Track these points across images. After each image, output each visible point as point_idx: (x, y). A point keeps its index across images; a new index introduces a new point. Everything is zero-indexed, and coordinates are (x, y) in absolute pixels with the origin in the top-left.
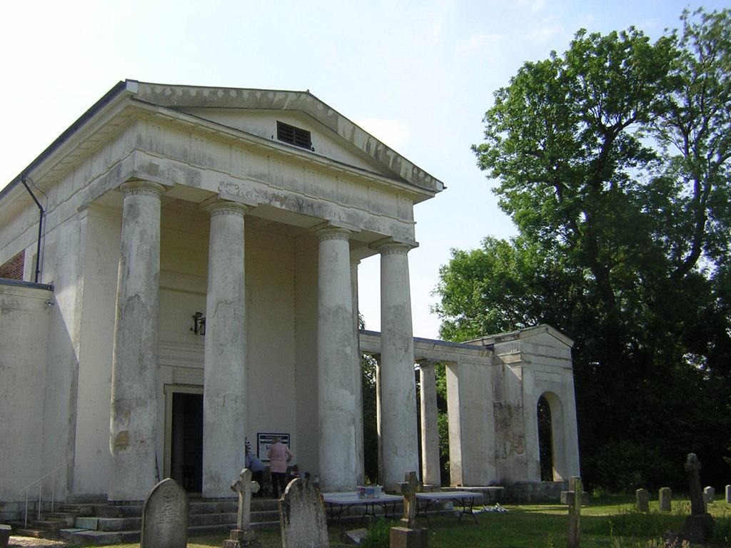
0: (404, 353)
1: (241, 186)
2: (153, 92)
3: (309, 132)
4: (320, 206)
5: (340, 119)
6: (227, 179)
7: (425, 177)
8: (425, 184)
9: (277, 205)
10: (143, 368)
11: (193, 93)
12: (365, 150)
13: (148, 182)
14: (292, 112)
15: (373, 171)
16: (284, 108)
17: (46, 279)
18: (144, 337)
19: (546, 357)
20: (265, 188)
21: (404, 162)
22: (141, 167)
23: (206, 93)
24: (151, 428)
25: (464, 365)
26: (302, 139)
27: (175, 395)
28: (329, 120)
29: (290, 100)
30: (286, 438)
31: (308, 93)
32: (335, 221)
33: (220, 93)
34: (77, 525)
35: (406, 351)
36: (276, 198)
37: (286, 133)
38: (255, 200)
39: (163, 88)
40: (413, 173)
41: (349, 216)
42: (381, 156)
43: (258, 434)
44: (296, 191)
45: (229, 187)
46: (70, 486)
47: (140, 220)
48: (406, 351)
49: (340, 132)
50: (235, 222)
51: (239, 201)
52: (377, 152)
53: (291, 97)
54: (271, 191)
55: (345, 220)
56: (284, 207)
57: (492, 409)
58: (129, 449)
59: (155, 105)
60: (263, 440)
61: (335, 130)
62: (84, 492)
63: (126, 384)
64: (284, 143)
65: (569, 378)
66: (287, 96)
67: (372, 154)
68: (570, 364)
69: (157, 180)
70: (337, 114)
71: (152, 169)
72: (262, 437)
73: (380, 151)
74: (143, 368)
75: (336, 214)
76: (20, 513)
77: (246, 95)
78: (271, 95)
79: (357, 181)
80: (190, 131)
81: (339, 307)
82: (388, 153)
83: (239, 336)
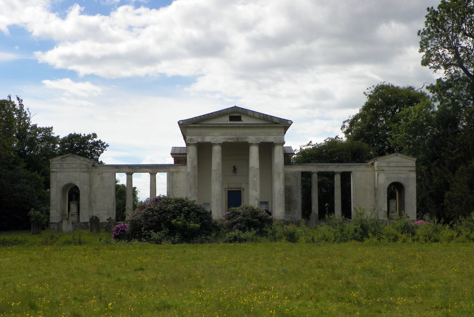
0: (278, 178)
2: (187, 121)
4: (245, 138)
5: (248, 111)
6: (212, 137)
9: (230, 141)
10: (191, 190)
11: (198, 118)
14: (230, 113)
16: (229, 112)
19: (395, 167)
21: (274, 118)
23: (202, 117)
26: (239, 119)
27: (228, 191)
28: (245, 112)
30: (267, 203)
35: (279, 177)
36: (229, 139)
37: (232, 118)
38: (221, 141)
48: (279, 177)
49: (249, 115)
51: (217, 143)
52: (263, 117)
54: (227, 137)
56: (232, 141)
65: (413, 175)
67: (262, 118)
68: (414, 169)
75: (251, 139)
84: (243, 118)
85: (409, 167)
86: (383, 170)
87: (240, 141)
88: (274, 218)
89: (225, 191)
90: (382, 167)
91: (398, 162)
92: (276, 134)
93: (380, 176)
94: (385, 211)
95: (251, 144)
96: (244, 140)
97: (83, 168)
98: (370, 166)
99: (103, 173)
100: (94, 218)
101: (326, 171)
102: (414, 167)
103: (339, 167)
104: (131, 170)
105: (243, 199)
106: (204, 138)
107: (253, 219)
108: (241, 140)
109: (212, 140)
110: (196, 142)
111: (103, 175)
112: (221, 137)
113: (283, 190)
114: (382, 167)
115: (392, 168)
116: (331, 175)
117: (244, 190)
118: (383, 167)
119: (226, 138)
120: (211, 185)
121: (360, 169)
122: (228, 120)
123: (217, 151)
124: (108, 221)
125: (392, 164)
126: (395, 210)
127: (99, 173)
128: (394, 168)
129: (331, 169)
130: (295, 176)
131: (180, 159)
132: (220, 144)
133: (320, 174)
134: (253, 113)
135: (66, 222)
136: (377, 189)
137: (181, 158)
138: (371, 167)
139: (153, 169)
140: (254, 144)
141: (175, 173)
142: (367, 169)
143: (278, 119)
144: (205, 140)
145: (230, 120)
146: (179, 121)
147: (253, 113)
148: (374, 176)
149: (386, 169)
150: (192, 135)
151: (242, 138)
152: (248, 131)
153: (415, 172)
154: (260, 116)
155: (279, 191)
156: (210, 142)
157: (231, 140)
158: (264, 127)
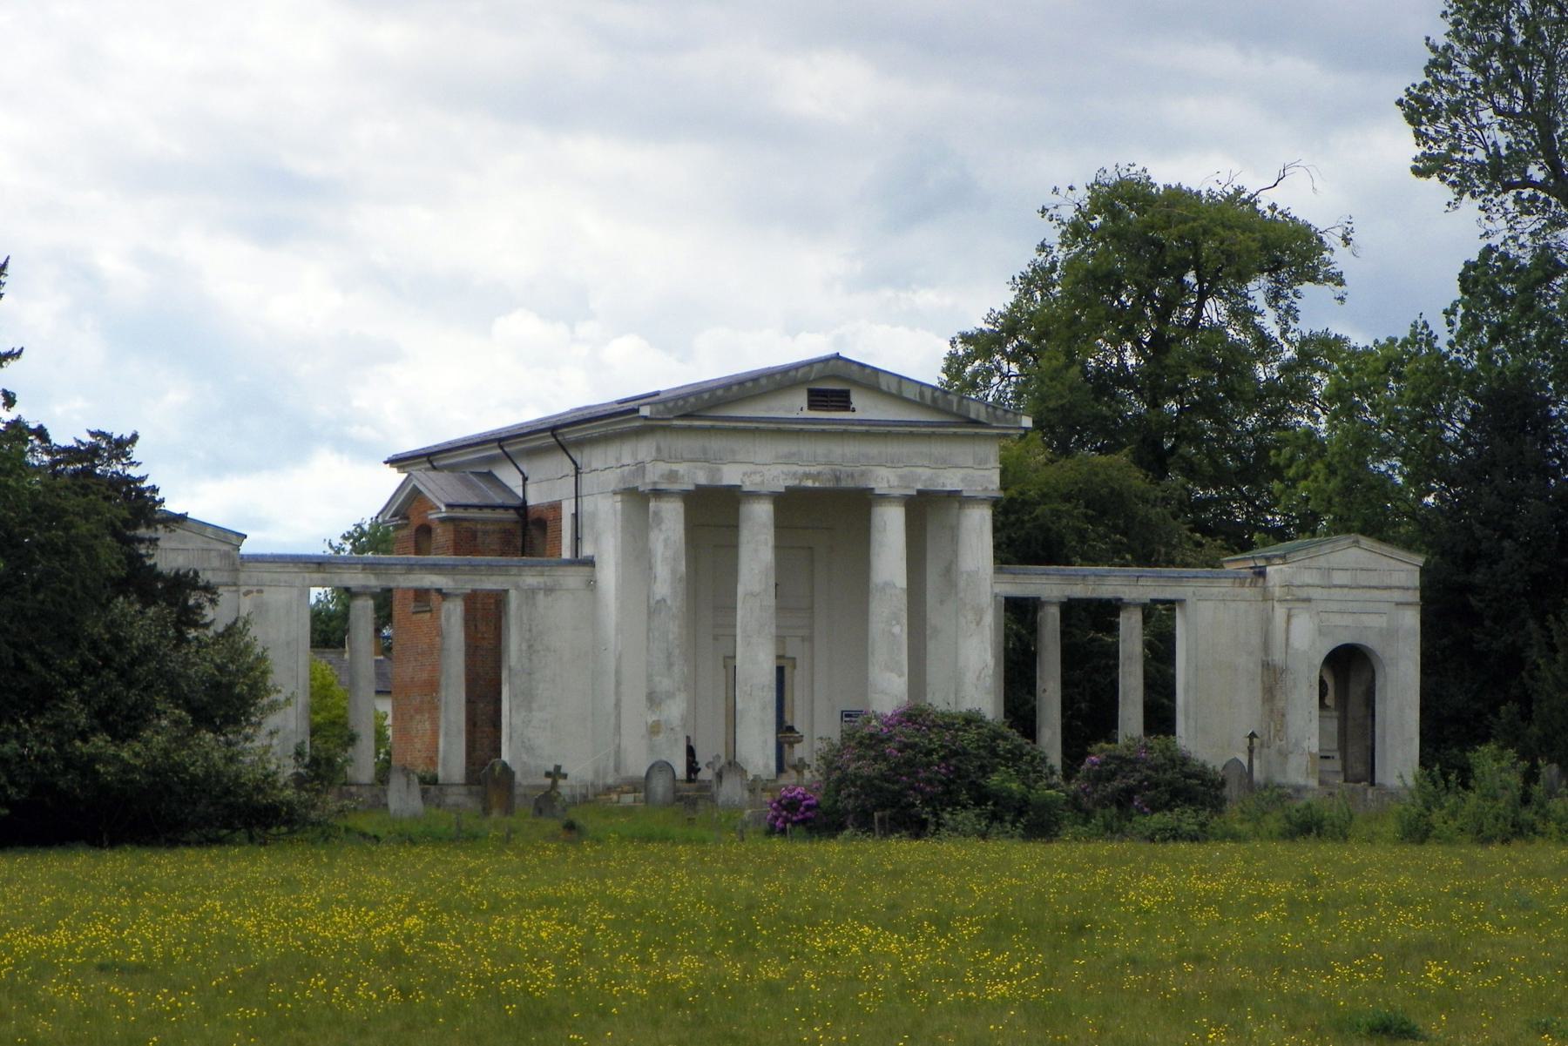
0: (973, 626)
4: (863, 474)
6: (751, 468)
9: (809, 483)
10: (670, 665)
17: (587, 550)
18: (671, 637)
19: (1350, 587)
22: (662, 476)
23: (720, 392)
25: (1200, 604)
26: (840, 400)
28: (871, 379)
31: (837, 357)
32: (880, 487)
35: (978, 624)
36: (807, 476)
37: (819, 399)
38: (780, 486)
41: (901, 477)
44: (832, 464)
45: (753, 477)
46: (617, 769)
47: (664, 527)
48: (978, 624)
49: (884, 387)
50: (760, 515)
51: (764, 489)
52: (934, 400)
53: (817, 367)
54: (801, 470)
55: (896, 484)
56: (817, 485)
57: (1259, 670)
58: (661, 735)
60: (848, 719)
62: (630, 774)
63: (657, 679)
65: (1411, 620)
68: (1415, 596)
69: (676, 487)
70: (876, 371)
71: (672, 476)
72: (847, 716)
74: (670, 665)
75: (884, 479)
76: (573, 797)
77: (763, 381)
78: (792, 373)
81: (887, 584)
84: (856, 399)
85: (1398, 588)
86: (1308, 600)
89: (725, 667)
90: (1302, 586)
91: (1362, 570)
92: (970, 464)
93: (1294, 621)
94: (1310, 753)
95: (884, 498)
96: (862, 484)
97: (213, 570)
98: (1249, 580)
99: (265, 589)
100: (497, 769)
101: (1095, 595)
102: (1415, 589)
103: (1142, 582)
104: (372, 577)
105: (793, 700)
106: (719, 470)
108: (847, 483)
110: (691, 487)
111: (265, 595)
112: (777, 470)
113: (991, 672)
114: (1302, 586)
115: (1336, 593)
116: (1104, 613)
117: (794, 667)
118: (1308, 586)
119: (795, 474)
120: (1035, 683)
121: (1215, 590)
122: (805, 405)
123: (759, 519)
124: (549, 781)
125: (1339, 578)
126: (1333, 751)
127: (247, 588)
128: (1346, 590)
129: (1110, 588)
131: (479, 526)
133: (1070, 608)
134: (877, 376)
135: (403, 780)
136: (1283, 671)
137: (484, 521)
138: (1253, 584)
139: (457, 577)
140: (894, 497)
141: (542, 592)
142: (1238, 590)
143: (896, 379)
144: (720, 480)
145: (812, 405)
148: (1267, 621)
149: (1315, 593)
150: (676, 458)
151: (852, 476)
152: (873, 449)
153: (1419, 608)
154: (922, 394)
155: (978, 678)
156: (740, 486)
157: (814, 483)
158: (930, 436)
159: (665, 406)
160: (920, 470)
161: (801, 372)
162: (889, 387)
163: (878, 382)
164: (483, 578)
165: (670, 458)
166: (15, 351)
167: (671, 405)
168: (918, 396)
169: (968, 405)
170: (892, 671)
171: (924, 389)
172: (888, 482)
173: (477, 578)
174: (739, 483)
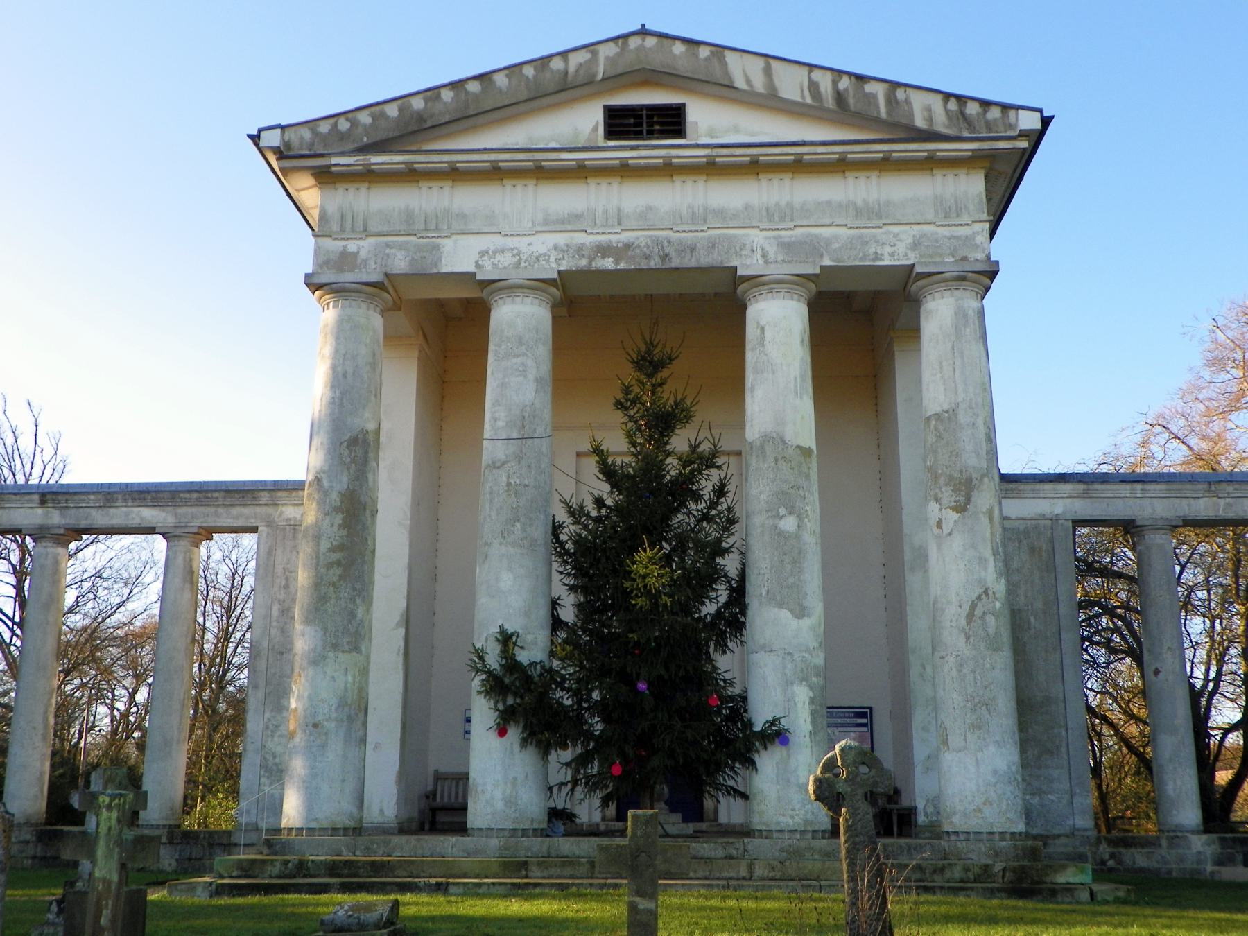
1: (524, 249)
2: (315, 133)
3: (684, 105)
5: (730, 57)
7: (985, 112)
8: (989, 126)
9: (608, 264)
12: (809, 100)
13: (334, 286)
14: (618, 80)
15: (886, 137)
16: (600, 77)
20: (580, 238)
23: (418, 104)
24: (334, 702)
29: (607, 58)
30: (863, 715)
31: (643, 32)
33: (447, 95)
34: (529, 876)
36: (604, 250)
39: (332, 121)
40: (947, 111)
42: (851, 101)
43: (870, 708)
45: (498, 257)
49: (740, 83)
51: (516, 276)
52: (840, 97)
54: (588, 240)
56: (622, 266)
59: (321, 156)
61: (726, 82)
64: (393, 166)
66: (595, 54)
67: (830, 102)
73: (846, 90)
77: (501, 80)
78: (557, 64)
79: (841, 166)
80: (410, 175)
82: (869, 88)
83: (518, 525)
87: (676, 262)
88: (542, 751)
107: (683, 904)
109: (486, 263)
130: (1032, 550)
132: (539, 285)
146: (260, 130)
147: (768, 71)
154: (814, 87)
155: (970, 617)
157: (617, 262)
159: (313, 131)
160: (826, 232)
161: (576, 60)
162: (748, 81)
163: (726, 73)
164: (220, 510)
165: (342, 230)
166: (564, 505)
167: (324, 128)
168: (807, 93)
169: (908, 102)
170: (780, 605)
171: (817, 75)
172: (764, 256)
173: (211, 510)
174: (472, 269)
